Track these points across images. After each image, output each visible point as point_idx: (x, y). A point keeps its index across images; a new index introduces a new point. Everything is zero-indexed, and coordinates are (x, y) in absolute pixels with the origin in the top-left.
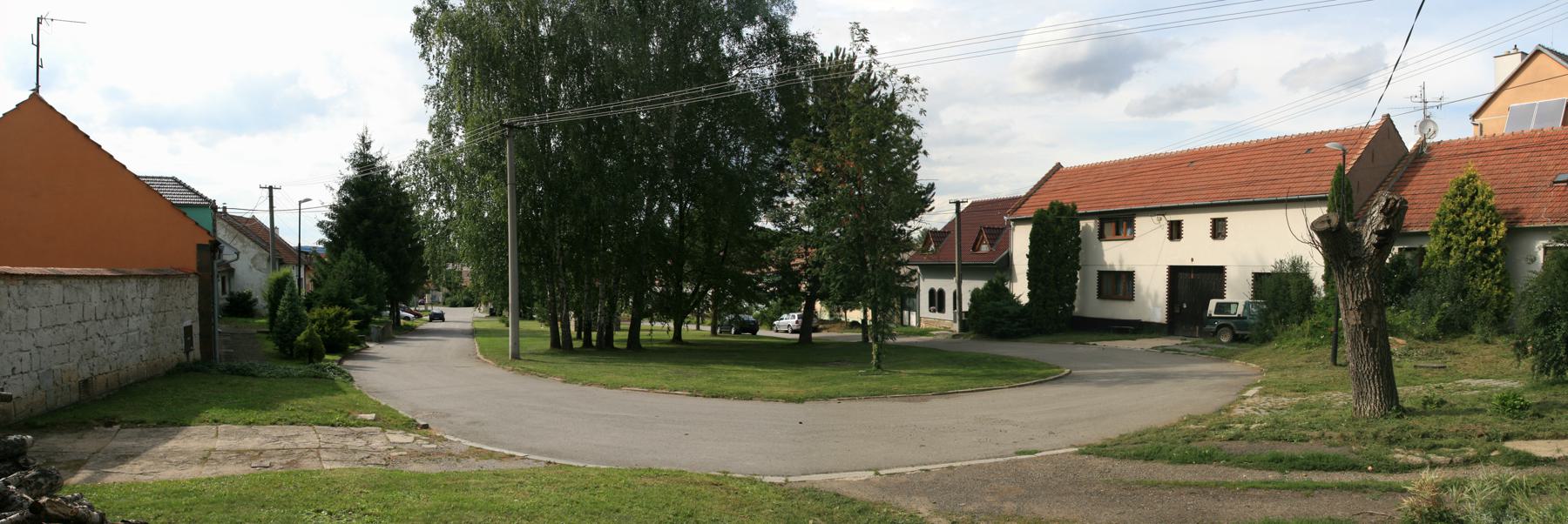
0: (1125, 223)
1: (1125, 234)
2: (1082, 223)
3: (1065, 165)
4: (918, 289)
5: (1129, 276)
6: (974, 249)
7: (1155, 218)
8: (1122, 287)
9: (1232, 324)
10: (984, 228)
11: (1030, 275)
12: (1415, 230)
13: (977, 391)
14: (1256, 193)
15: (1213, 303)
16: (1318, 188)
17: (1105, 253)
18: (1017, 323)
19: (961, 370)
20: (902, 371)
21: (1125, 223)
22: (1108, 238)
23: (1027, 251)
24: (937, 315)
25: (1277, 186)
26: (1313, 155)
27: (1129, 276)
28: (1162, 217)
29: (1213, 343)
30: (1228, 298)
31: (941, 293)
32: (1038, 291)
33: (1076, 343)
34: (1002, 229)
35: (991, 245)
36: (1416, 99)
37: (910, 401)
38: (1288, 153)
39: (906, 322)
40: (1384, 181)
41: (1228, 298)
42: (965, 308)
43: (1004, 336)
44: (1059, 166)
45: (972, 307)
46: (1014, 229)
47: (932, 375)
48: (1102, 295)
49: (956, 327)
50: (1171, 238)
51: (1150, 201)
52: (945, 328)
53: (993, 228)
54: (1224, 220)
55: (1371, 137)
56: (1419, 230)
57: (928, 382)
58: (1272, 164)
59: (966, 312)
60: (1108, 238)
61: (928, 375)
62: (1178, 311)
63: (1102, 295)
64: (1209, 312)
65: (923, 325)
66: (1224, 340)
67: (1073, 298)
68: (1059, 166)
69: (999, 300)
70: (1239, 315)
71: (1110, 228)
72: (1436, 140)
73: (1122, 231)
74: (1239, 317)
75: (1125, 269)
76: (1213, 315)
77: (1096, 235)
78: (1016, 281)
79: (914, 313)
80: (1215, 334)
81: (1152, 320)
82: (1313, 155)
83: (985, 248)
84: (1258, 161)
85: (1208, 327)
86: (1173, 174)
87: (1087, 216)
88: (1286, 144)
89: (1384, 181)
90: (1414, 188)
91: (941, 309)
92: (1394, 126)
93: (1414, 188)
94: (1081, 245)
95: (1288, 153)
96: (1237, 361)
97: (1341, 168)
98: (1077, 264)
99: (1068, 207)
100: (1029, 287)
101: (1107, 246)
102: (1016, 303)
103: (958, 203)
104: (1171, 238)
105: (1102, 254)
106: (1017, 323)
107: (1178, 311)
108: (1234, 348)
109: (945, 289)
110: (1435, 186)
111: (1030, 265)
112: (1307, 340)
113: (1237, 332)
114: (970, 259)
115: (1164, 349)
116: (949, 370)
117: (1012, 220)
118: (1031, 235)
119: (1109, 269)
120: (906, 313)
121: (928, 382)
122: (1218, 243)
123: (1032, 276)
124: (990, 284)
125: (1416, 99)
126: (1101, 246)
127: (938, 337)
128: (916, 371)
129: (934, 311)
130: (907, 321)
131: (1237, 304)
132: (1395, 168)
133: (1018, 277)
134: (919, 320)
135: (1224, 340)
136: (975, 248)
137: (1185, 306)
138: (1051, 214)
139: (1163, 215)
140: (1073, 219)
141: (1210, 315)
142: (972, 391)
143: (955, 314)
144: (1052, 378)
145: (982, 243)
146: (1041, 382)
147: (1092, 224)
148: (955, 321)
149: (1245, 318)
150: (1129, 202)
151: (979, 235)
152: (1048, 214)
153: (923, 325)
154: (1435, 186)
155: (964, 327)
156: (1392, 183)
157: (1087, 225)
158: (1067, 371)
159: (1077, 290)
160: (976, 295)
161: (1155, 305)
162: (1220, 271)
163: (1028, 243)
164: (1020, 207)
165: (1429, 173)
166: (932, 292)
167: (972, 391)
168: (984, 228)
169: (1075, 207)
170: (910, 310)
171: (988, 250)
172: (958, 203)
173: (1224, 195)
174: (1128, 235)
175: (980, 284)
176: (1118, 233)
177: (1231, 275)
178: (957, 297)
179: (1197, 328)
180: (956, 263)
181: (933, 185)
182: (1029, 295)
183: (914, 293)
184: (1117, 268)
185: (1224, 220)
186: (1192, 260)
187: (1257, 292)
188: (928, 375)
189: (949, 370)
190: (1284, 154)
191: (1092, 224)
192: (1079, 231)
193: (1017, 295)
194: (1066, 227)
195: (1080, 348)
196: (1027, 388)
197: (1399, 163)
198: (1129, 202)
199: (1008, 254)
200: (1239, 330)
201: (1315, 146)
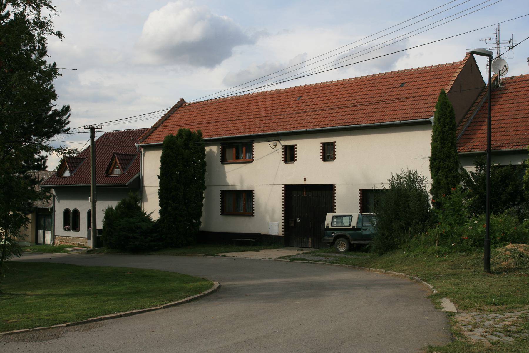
0: (244, 149)
1: (245, 158)
2: (207, 149)
3: (188, 101)
4: (53, 209)
5: (249, 194)
6: (107, 172)
7: (272, 143)
8: (242, 204)
9: (348, 236)
10: (117, 154)
11: (161, 194)
12: (509, 149)
13: (126, 315)
14: (362, 120)
15: (329, 216)
16: (417, 115)
17: (227, 175)
18: (150, 238)
19: (101, 288)
20: (29, 293)
21: (244, 149)
22: (229, 161)
23: (159, 172)
24: (72, 233)
25: (379, 114)
26: (407, 88)
27: (249, 194)
28: (277, 142)
29: (330, 252)
30: (339, 212)
31: (76, 213)
32: (169, 208)
33: (206, 255)
34: (133, 155)
35: (123, 169)
36: (490, 42)
37: (32, 340)
38: (384, 87)
39: (41, 240)
40: (469, 110)
41: (339, 212)
42: (100, 225)
43: (137, 250)
44: (182, 101)
45: (106, 224)
46: (144, 155)
47: (66, 295)
48: (224, 212)
49: (90, 244)
50: (286, 161)
51: (267, 128)
52: (79, 245)
53: (125, 155)
54: (333, 144)
55: (460, 70)
56: (512, 149)
57: (61, 306)
58: (371, 96)
59: (100, 230)
60: (229, 161)
61: (62, 295)
62: (293, 225)
63: (224, 212)
64: (326, 225)
65: (57, 243)
66: (341, 249)
67: (199, 214)
68: (182, 101)
69: (132, 217)
70: (354, 227)
71: (231, 153)
72: (509, 75)
73: (242, 156)
74: (354, 228)
75: (245, 188)
76: (330, 227)
77: (219, 159)
78: (147, 201)
79: (50, 232)
80: (332, 244)
81: (270, 233)
82: (407, 88)
83: (117, 172)
84: (358, 94)
85: (326, 238)
86: (285, 107)
87: (211, 142)
88: (382, 81)
89: (469, 110)
90: (498, 114)
91: (76, 227)
92: (476, 62)
93: (498, 114)
94: (206, 168)
95: (384, 87)
96: (374, 269)
97: (443, 93)
98: (203, 185)
99: (195, 134)
100: (161, 205)
101: (229, 168)
102: (148, 219)
103: (92, 130)
104: (286, 161)
105: (224, 175)
106: (150, 238)
107: (293, 225)
108: (352, 256)
109: (79, 209)
110: (517, 112)
111: (161, 184)
112: (437, 248)
113: (353, 242)
114: (104, 182)
115: (292, 259)
116: (87, 288)
117: (143, 147)
118: (162, 158)
119: (230, 189)
120: (41, 232)
121: (61, 306)
122: (328, 164)
123: (163, 194)
124: (124, 203)
125: (490, 42)
126: (224, 169)
127: (72, 253)
128: (47, 291)
129: (69, 230)
130: (42, 240)
131: (352, 216)
132: (477, 99)
133: (149, 197)
134: (53, 238)
135: (341, 249)
136: (109, 172)
137: (299, 221)
138: (179, 139)
139: (279, 141)
140: (199, 145)
141: (328, 227)
142: (121, 316)
143: (89, 232)
144: (206, 292)
145: (115, 168)
146: (196, 299)
147: (215, 149)
148: (89, 238)
149: (359, 229)
150: (248, 130)
151: (112, 160)
152: (177, 139)
153: (57, 243)
154: (517, 112)
155: (98, 243)
156: (475, 113)
157: (211, 150)
158: (216, 284)
159: (203, 208)
160: (109, 213)
161: (273, 219)
162: (330, 189)
163: (159, 164)
164: (149, 135)
165: (507, 102)
166: (67, 212)
167: (121, 316)
168: (117, 154)
169: (200, 134)
170: (45, 229)
171: (120, 173)
172: (92, 130)
173: (332, 122)
174: (247, 158)
175: (114, 204)
176: (238, 158)
177: (339, 192)
178: (91, 216)
179: (310, 239)
180: (91, 185)
181: (68, 107)
182: (161, 212)
183: (49, 213)
184: (238, 188)
185: (333, 144)
186: (305, 179)
187: (364, 207)
188: (62, 295)
189: (87, 288)
190: (380, 88)
191: (215, 149)
192: (204, 156)
193: (148, 213)
194: (193, 151)
195: (211, 260)
196: (185, 308)
197: (479, 95)
198: (248, 130)
199: (139, 176)
200: (355, 240)
201: (408, 81)
